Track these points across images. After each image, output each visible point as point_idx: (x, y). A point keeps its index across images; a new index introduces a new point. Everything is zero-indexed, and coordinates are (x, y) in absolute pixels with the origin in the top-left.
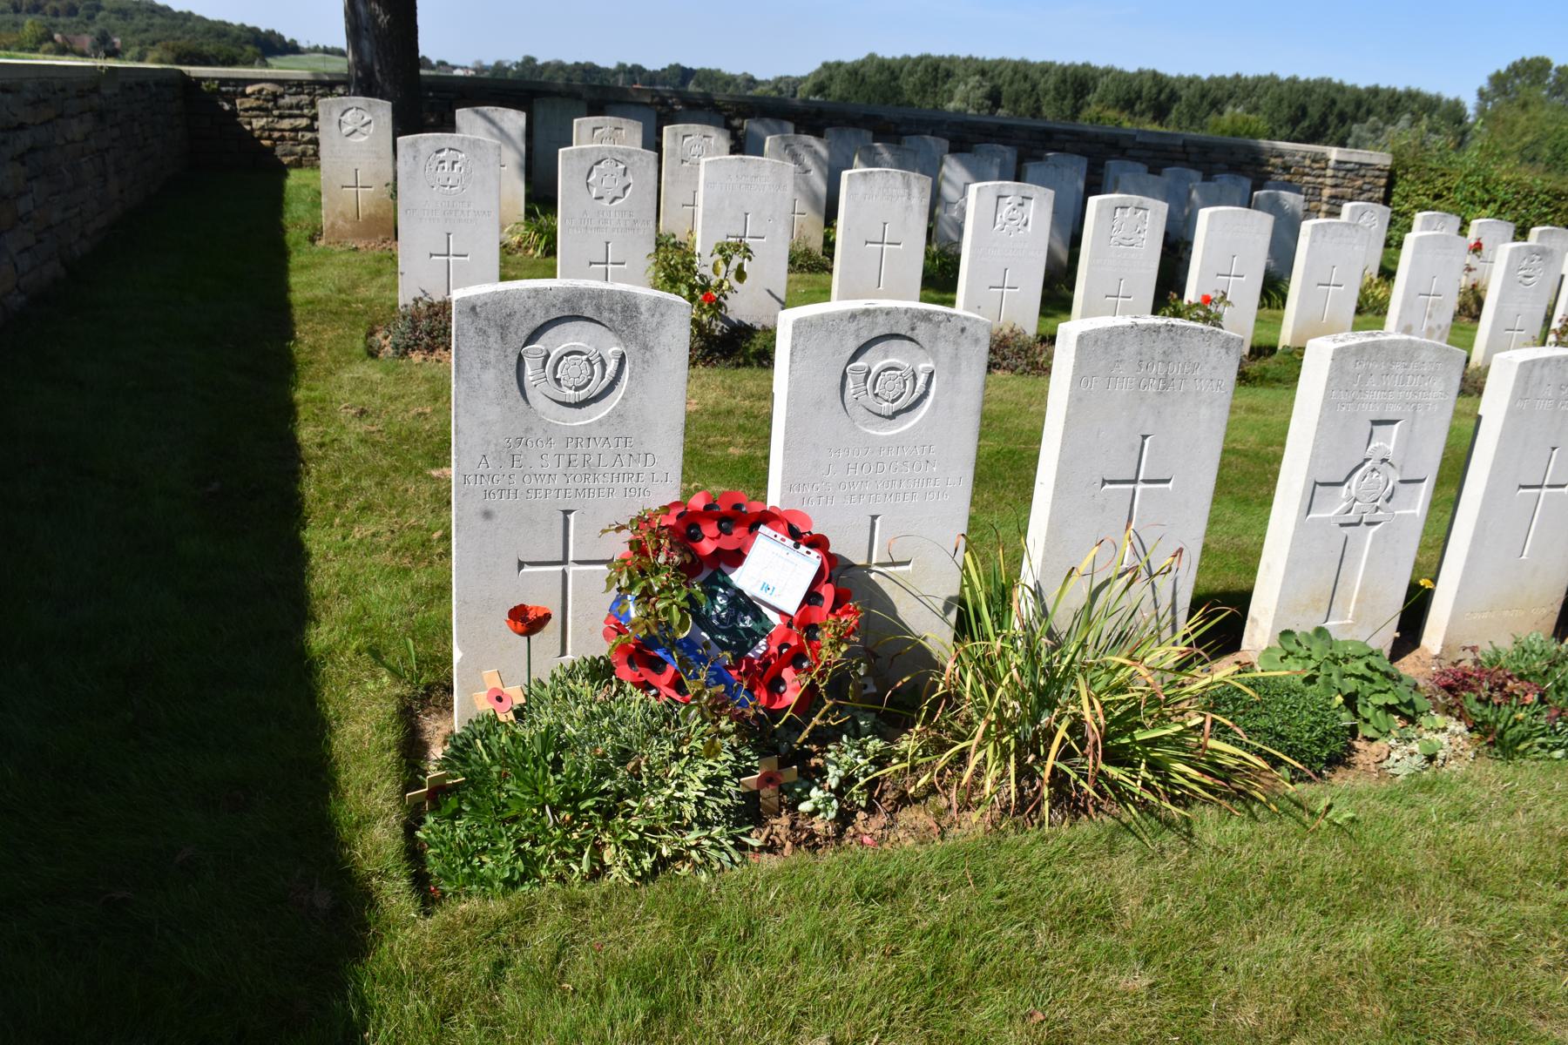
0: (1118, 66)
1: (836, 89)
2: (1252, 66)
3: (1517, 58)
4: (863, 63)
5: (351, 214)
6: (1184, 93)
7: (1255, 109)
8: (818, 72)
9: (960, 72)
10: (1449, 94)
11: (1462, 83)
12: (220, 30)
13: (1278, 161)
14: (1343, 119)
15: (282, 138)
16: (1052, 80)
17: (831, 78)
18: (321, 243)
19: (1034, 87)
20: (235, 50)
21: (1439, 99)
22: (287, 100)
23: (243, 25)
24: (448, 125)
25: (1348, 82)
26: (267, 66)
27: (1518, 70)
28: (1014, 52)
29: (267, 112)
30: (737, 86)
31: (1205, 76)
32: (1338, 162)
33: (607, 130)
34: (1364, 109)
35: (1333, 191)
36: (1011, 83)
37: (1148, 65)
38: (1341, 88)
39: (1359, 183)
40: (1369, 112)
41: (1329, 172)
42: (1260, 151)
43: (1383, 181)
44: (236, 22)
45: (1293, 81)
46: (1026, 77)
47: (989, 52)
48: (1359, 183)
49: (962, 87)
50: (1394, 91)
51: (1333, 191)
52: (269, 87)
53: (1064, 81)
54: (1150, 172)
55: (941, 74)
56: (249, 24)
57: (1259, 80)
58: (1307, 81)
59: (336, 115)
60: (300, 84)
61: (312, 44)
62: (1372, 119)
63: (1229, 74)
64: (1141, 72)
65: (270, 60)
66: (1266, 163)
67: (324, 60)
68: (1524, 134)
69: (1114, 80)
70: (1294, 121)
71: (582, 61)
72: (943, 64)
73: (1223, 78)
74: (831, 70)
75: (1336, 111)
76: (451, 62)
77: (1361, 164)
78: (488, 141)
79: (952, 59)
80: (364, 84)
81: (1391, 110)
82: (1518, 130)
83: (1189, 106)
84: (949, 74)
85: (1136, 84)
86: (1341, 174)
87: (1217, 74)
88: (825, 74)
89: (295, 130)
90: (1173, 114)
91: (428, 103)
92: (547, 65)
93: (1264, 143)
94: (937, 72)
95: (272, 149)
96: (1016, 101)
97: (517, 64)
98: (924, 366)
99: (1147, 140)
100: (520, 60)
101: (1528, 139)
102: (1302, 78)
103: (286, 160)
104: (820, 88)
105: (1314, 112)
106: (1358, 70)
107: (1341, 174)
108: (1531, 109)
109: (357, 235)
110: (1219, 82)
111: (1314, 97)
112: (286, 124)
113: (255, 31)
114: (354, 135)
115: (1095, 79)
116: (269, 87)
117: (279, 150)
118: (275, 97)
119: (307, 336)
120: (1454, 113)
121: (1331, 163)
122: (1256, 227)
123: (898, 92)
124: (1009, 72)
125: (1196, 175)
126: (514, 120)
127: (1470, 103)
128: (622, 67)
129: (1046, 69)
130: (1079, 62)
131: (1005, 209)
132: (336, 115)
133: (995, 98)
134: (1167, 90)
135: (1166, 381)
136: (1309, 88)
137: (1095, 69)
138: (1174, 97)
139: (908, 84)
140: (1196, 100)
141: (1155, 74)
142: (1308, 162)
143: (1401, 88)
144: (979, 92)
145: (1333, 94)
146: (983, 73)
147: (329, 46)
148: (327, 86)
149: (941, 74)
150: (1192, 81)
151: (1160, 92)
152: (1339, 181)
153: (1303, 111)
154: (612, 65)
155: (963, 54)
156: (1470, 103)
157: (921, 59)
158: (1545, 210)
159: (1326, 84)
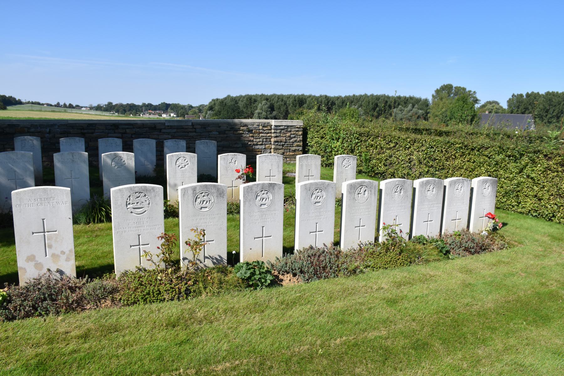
0: (313, 94)
2: (359, 91)
3: (442, 85)
4: (225, 99)
6: (336, 102)
8: (211, 102)
9: (259, 99)
10: (423, 97)
11: (426, 92)
13: (245, 128)
14: (390, 107)
17: (215, 104)
19: (285, 104)
21: (420, 99)
27: (460, 91)
28: (279, 91)
32: (276, 126)
34: (397, 104)
35: (276, 139)
36: (277, 102)
37: (323, 93)
38: (388, 97)
39: (288, 134)
40: (399, 104)
41: (273, 131)
42: (235, 124)
43: (300, 133)
45: (372, 95)
46: (282, 100)
48: (288, 134)
49: (260, 105)
50: (406, 97)
51: (276, 139)
55: (253, 100)
57: (361, 96)
58: (377, 95)
61: (27, 101)
62: (400, 106)
63: (351, 95)
64: (321, 96)
65: (8, 107)
66: (239, 129)
67: (32, 106)
68: (442, 108)
70: (374, 109)
71: (130, 103)
72: (253, 97)
76: (81, 105)
77: (288, 126)
81: (405, 103)
82: (440, 107)
84: (255, 101)
86: (278, 131)
87: (347, 95)
88: (213, 103)
92: (116, 105)
96: (279, 108)
97: (106, 105)
99: (171, 124)
100: (107, 104)
101: (444, 110)
102: (375, 94)
104: (211, 108)
107: (278, 131)
108: (444, 100)
111: (380, 100)
120: (425, 103)
121: (273, 127)
122: (240, 160)
124: (276, 99)
127: (430, 99)
128: (144, 104)
129: (289, 97)
130: (300, 94)
136: (378, 98)
138: (333, 104)
139: (241, 104)
141: (326, 96)
142: (261, 127)
143: (408, 96)
145: (386, 99)
146: (267, 99)
147: (34, 101)
149: (253, 100)
150: (338, 98)
152: (278, 135)
153: (377, 105)
154: (141, 104)
155: (260, 94)
156: (430, 99)
157: (246, 96)
158: (357, 141)
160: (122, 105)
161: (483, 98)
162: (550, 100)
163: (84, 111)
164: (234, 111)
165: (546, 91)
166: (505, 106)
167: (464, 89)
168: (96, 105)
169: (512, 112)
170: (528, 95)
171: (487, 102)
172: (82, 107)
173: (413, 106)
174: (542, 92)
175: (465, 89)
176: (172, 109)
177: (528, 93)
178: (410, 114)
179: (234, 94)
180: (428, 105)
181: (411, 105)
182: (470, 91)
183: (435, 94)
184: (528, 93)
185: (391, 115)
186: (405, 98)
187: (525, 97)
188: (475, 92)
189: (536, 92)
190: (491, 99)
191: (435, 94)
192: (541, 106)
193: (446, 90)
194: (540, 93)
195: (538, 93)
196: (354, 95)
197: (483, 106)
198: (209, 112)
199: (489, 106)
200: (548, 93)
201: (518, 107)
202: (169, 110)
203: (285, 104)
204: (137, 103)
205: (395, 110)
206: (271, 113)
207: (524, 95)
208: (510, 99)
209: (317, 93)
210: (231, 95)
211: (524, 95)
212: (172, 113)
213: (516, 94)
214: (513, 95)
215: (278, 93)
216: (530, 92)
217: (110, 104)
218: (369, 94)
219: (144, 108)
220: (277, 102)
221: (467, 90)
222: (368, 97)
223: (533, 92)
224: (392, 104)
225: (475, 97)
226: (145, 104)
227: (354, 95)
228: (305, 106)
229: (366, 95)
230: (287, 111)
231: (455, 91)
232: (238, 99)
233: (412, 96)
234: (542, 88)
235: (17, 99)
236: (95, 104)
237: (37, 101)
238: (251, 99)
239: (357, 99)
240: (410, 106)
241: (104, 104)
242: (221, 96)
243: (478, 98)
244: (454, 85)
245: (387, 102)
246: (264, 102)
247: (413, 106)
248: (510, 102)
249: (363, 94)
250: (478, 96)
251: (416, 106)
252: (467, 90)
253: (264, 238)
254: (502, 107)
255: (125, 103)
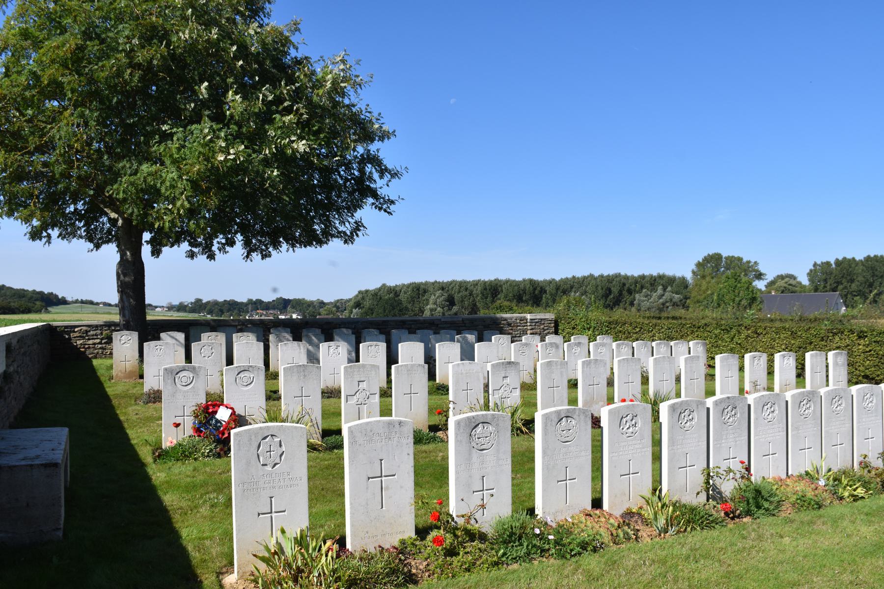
1: (367, 304)
2: (580, 270)
3: (706, 254)
4: (380, 289)
5: (123, 371)
6: (547, 289)
7: (585, 293)
8: (357, 296)
10: (679, 274)
11: (683, 267)
12: (21, 294)
13: (505, 322)
14: (630, 292)
15: (89, 348)
16: (479, 288)
17: (363, 298)
18: (113, 381)
19: (471, 294)
20: (30, 305)
22: (92, 333)
23: (34, 291)
24: (159, 339)
25: (629, 274)
26: (49, 312)
27: (734, 263)
29: (83, 338)
30: (314, 307)
31: (558, 279)
33: (213, 337)
36: (459, 292)
38: (626, 277)
40: (642, 287)
42: (497, 319)
44: (30, 289)
46: (466, 289)
47: (445, 277)
52: (84, 328)
53: (485, 289)
54: (409, 333)
56: (38, 290)
57: (584, 278)
58: (608, 276)
59: (119, 338)
60: (97, 326)
61: (75, 299)
62: (644, 291)
63: (570, 276)
64: (524, 280)
65: (49, 309)
69: (511, 285)
70: (606, 296)
72: (422, 286)
73: (567, 278)
74: (364, 294)
75: (626, 288)
78: (172, 341)
79: (426, 283)
80: (127, 327)
81: (652, 285)
83: (551, 295)
84: (425, 291)
85: (522, 286)
88: (360, 296)
89: (94, 344)
90: (544, 300)
91: (149, 331)
92: (208, 302)
93: (498, 315)
94: (419, 291)
95: (85, 352)
96: (462, 301)
97: (192, 303)
98: (252, 376)
102: (605, 274)
103: (90, 356)
104: (358, 305)
105: (615, 290)
106: (633, 268)
109: (125, 378)
110: (565, 281)
112: (91, 342)
113: (41, 293)
114: (125, 344)
115: (501, 286)
116: (84, 328)
117: (87, 352)
118: (87, 332)
119: (115, 402)
120: (683, 282)
123: (400, 303)
125: (431, 332)
126: (181, 336)
127: (689, 276)
128: (250, 301)
129: (476, 283)
130: (493, 279)
131: (331, 350)
132: (119, 338)
133: (451, 301)
134: (539, 289)
135: (305, 376)
136: (610, 279)
137: (501, 281)
138: (543, 291)
139: (403, 297)
140: (554, 292)
143: (655, 274)
144: (442, 299)
148: (111, 326)
150: (551, 282)
151: (535, 289)
153: (609, 291)
154: (245, 300)
155: (432, 280)
156: (689, 276)
159: (618, 276)
160: (216, 303)
161: (771, 270)
162: (873, 268)
163: (158, 312)
164: (394, 309)
165: (865, 255)
166: (805, 281)
167: (740, 259)
168: (178, 303)
169: (816, 290)
170: (838, 262)
171: (778, 276)
172: (156, 307)
173: (665, 289)
174: (860, 256)
175: (742, 259)
176: (293, 307)
177: (837, 259)
178: (661, 301)
179: (391, 283)
180: (686, 287)
181: (661, 287)
182: (749, 262)
183: (696, 270)
184: (837, 259)
185: (632, 304)
186: (651, 276)
187: (834, 266)
188: (755, 263)
189: (849, 257)
190: (783, 272)
191: (696, 270)
192: (860, 278)
193: (712, 264)
194: (857, 259)
195: (854, 258)
196: (574, 277)
197: (772, 283)
198: (354, 311)
199: (781, 283)
200: (868, 258)
201: (825, 281)
202: (289, 309)
203: (471, 294)
204: (239, 300)
205: (637, 296)
206: (450, 309)
207: (832, 262)
208: (811, 271)
209: (518, 276)
210: (388, 284)
211: (832, 262)
212: (294, 313)
213: (819, 262)
214: (815, 265)
215: (459, 278)
216: (840, 258)
217: (198, 301)
218: (596, 274)
219: (250, 307)
220: (459, 292)
221: (745, 260)
222: (596, 279)
223: (845, 258)
224: (632, 287)
225: (757, 271)
226: (251, 300)
227: (574, 277)
228: (501, 296)
229: (591, 276)
230: (475, 305)
231: (726, 262)
232: (398, 289)
233: (661, 273)
234: (859, 249)
235: (60, 297)
236: (176, 302)
237: (89, 299)
238: (418, 289)
239: (578, 283)
240: (660, 290)
241: (189, 301)
242: (373, 285)
243: (763, 271)
244: (724, 255)
245: (624, 284)
246: (438, 293)
247: (665, 289)
248: (812, 274)
249: (586, 274)
250: (762, 268)
251: (669, 288)
252: (745, 260)
253: (568, 482)
254: (800, 283)
255: (221, 299)
